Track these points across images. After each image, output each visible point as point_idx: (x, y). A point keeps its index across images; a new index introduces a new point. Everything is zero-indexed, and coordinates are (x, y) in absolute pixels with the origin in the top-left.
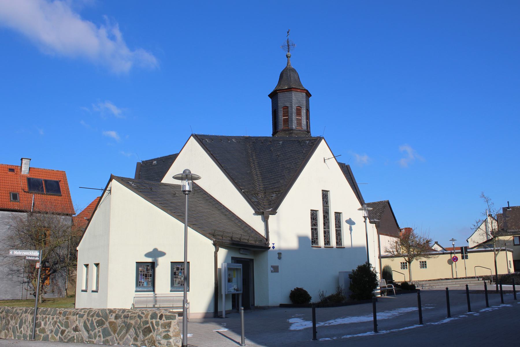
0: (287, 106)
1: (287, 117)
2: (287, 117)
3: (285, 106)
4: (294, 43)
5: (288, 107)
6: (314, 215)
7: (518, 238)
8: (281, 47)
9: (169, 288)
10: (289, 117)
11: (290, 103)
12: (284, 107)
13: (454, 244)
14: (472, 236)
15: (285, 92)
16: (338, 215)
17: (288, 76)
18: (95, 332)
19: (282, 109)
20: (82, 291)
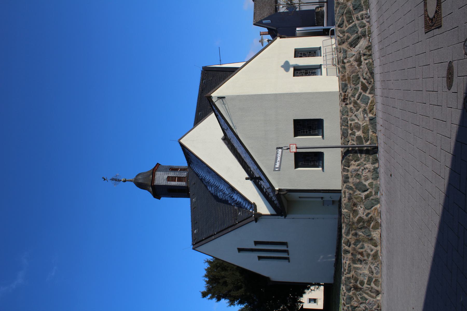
0: (167, 177)
1: (177, 178)
2: (177, 178)
3: (167, 179)
4: (115, 175)
5: (168, 177)
6: (260, 258)
7: (294, 154)
8: (115, 186)
9: (319, 57)
10: (177, 176)
11: (165, 175)
12: (167, 180)
13: (282, 6)
14: (209, 242)
15: (155, 178)
16: (256, 243)
17: (142, 178)
18: (355, 120)
19: (169, 182)
20: (322, 75)
